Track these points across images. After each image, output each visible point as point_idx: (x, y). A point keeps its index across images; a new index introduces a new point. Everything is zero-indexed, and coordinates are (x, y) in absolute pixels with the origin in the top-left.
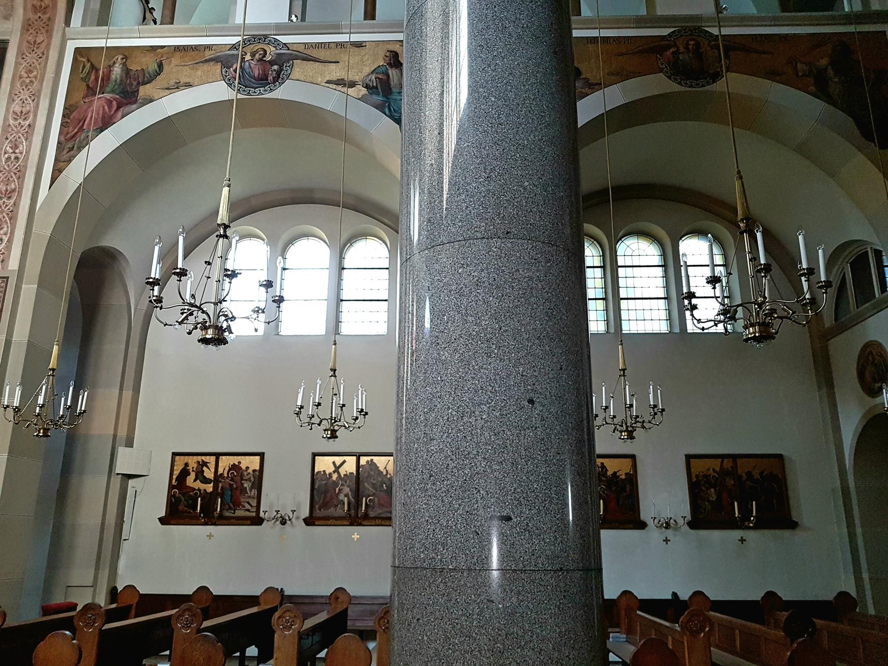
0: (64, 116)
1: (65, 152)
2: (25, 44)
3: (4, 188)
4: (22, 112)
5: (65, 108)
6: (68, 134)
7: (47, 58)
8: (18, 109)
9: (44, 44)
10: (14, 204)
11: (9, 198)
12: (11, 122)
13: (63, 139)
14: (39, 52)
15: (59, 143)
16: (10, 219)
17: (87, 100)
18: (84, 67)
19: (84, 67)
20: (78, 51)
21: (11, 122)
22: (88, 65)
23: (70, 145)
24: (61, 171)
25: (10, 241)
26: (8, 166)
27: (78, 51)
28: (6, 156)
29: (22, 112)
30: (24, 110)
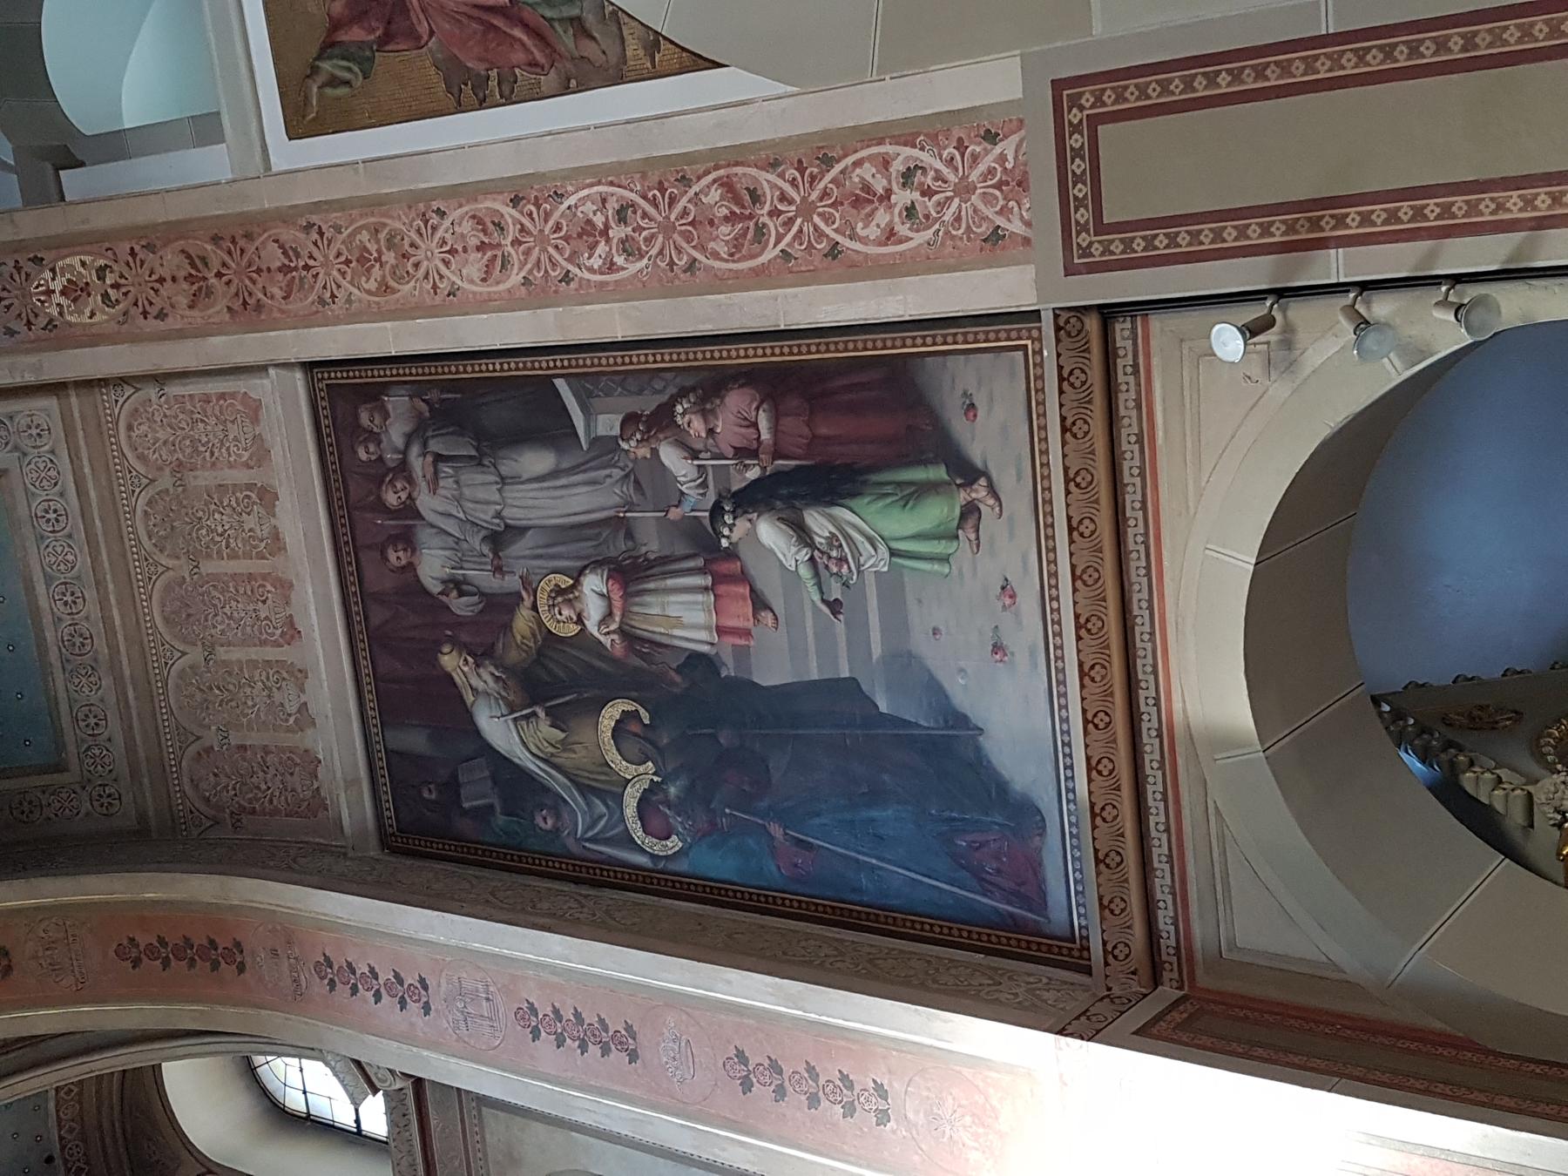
0: (482, 104)
1: (589, 49)
2: (298, 305)
3: (725, 229)
4: (482, 247)
5: (460, 108)
6: (533, 64)
7: (317, 207)
8: (474, 265)
9: (289, 235)
10: (773, 165)
11: (756, 197)
12: (516, 278)
13: (550, 80)
14: (305, 242)
15: (565, 90)
16: (828, 162)
17: (423, 29)
18: (334, 82)
19: (334, 82)
20: (298, 127)
21: (516, 278)
22: (326, 66)
23: (566, 39)
24: (654, 41)
25: (907, 133)
26: (649, 240)
27: (298, 127)
28: (619, 260)
29: (482, 247)
30: (474, 242)
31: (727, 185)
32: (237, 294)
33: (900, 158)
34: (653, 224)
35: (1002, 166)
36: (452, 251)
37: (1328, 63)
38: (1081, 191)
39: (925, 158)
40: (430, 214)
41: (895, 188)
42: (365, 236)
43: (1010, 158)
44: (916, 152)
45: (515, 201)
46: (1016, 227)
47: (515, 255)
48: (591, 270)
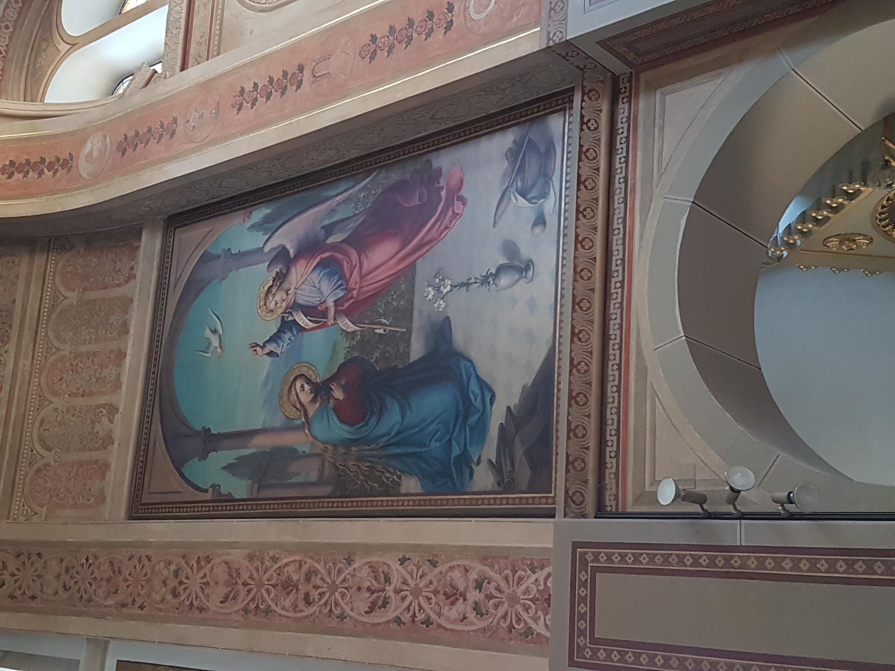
31: (372, 567)
32: (131, 594)
33: (475, 571)
34: (325, 585)
35: (537, 587)
36: (207, 584)
37: (732, 562)
38: (583, 608)
39: (319, 567)
40: (267, 558)
41: (471, 589)
42: (457, 575)
43: (542, 583)
44: (486, 568)
45: (403, 561)
46: (539, 628)
47: (394, 599)
48: (448, 619)
